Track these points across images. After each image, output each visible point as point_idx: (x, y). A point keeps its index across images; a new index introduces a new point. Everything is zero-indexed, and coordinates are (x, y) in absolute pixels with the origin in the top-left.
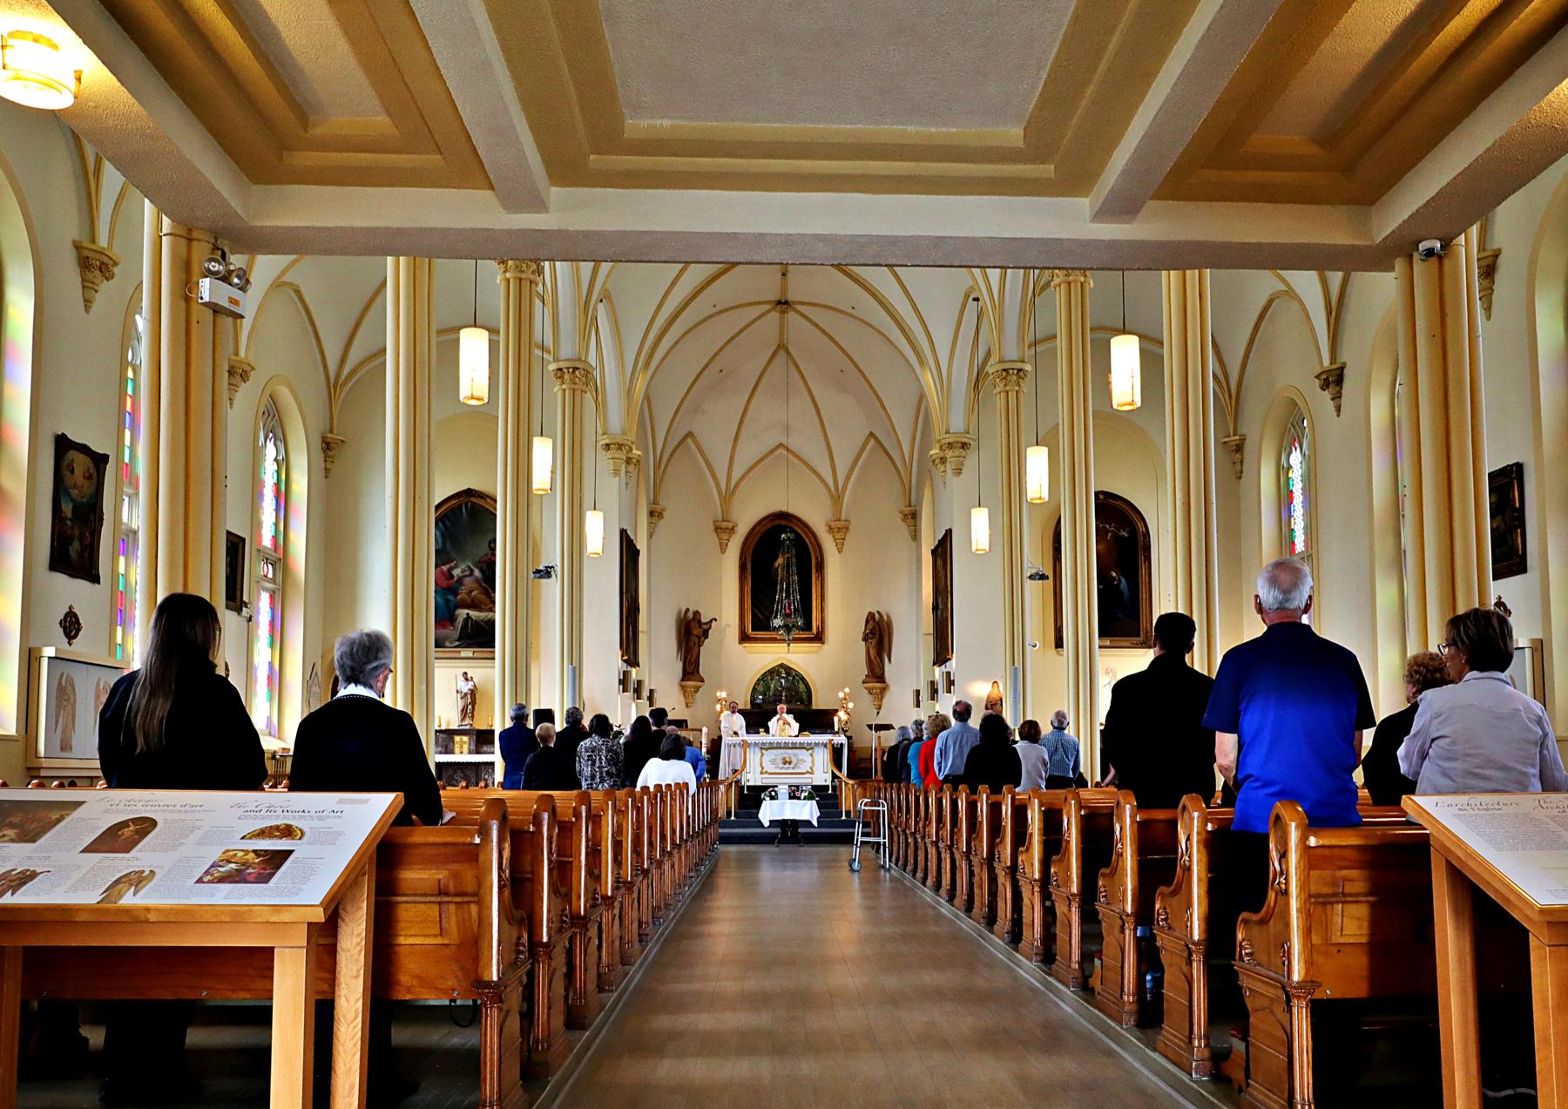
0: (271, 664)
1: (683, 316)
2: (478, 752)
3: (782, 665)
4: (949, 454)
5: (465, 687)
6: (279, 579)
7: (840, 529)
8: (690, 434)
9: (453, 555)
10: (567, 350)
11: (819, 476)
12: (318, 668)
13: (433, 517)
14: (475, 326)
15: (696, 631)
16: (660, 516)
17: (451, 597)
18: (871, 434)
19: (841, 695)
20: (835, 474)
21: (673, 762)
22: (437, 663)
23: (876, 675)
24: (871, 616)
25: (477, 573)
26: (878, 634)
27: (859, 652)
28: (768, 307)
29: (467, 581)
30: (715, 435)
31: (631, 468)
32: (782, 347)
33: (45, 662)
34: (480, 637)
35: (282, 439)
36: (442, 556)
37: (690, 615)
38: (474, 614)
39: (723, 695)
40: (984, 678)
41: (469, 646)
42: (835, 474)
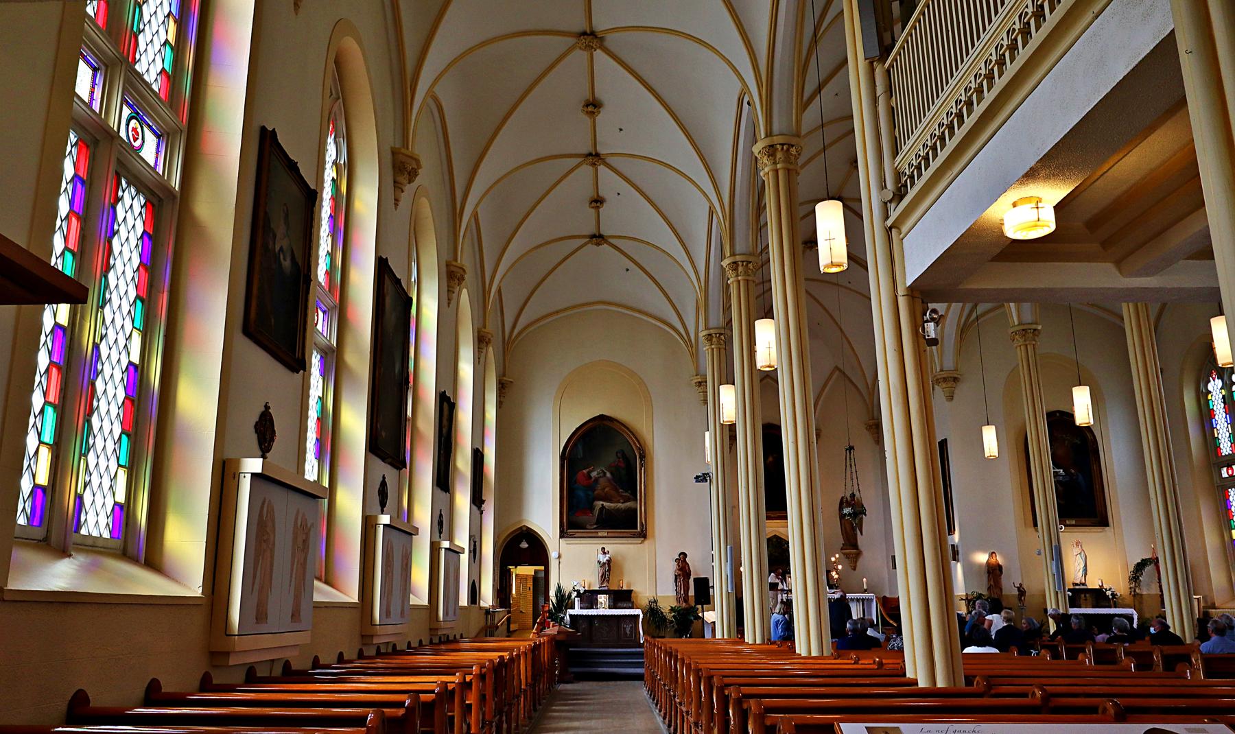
2: (616, 608)
5: (604, 559)
11: (856, 387)
20: (514, 327)
21: (255, 436)
25: (608, 475)
29: (601, 480)
33: (380, 530)
40: (984, 550)
42: (514, 327)
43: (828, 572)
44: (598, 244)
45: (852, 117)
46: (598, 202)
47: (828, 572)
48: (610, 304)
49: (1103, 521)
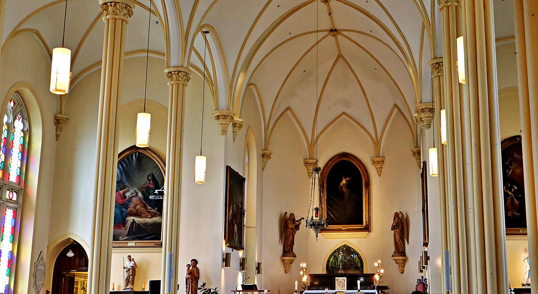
0: (12, 253)
1: (269, 39)
3: (345, 246)
4: (422, 115)
5: (129, 265)
6: (21, 201)
7: (379, 162)
8: (289, 108)
9: (127, 184)
10: (174, 62)
12: (44, 255)
13: (117, 160)
14: (63, 47)
15: (291, 226)
16: (269, 156)
17: (124, 210)
18: (395, 105)
19: (376, 265)
22: (114, 250)
23: (400, 251)
24: (396, 215)
25: (140, 195)
26: (401, 225)
27: (390, 236)
28: (326, 33)
29: (134, 199)
30: (303, 106)
31: (236, 129)
32: (340, 56)
34: (150, 234)
35: (27, 119)
36: (120, 185)
37: (288, 215)
38: (137, 220)
39: (304, 265)
41: (133, 239)
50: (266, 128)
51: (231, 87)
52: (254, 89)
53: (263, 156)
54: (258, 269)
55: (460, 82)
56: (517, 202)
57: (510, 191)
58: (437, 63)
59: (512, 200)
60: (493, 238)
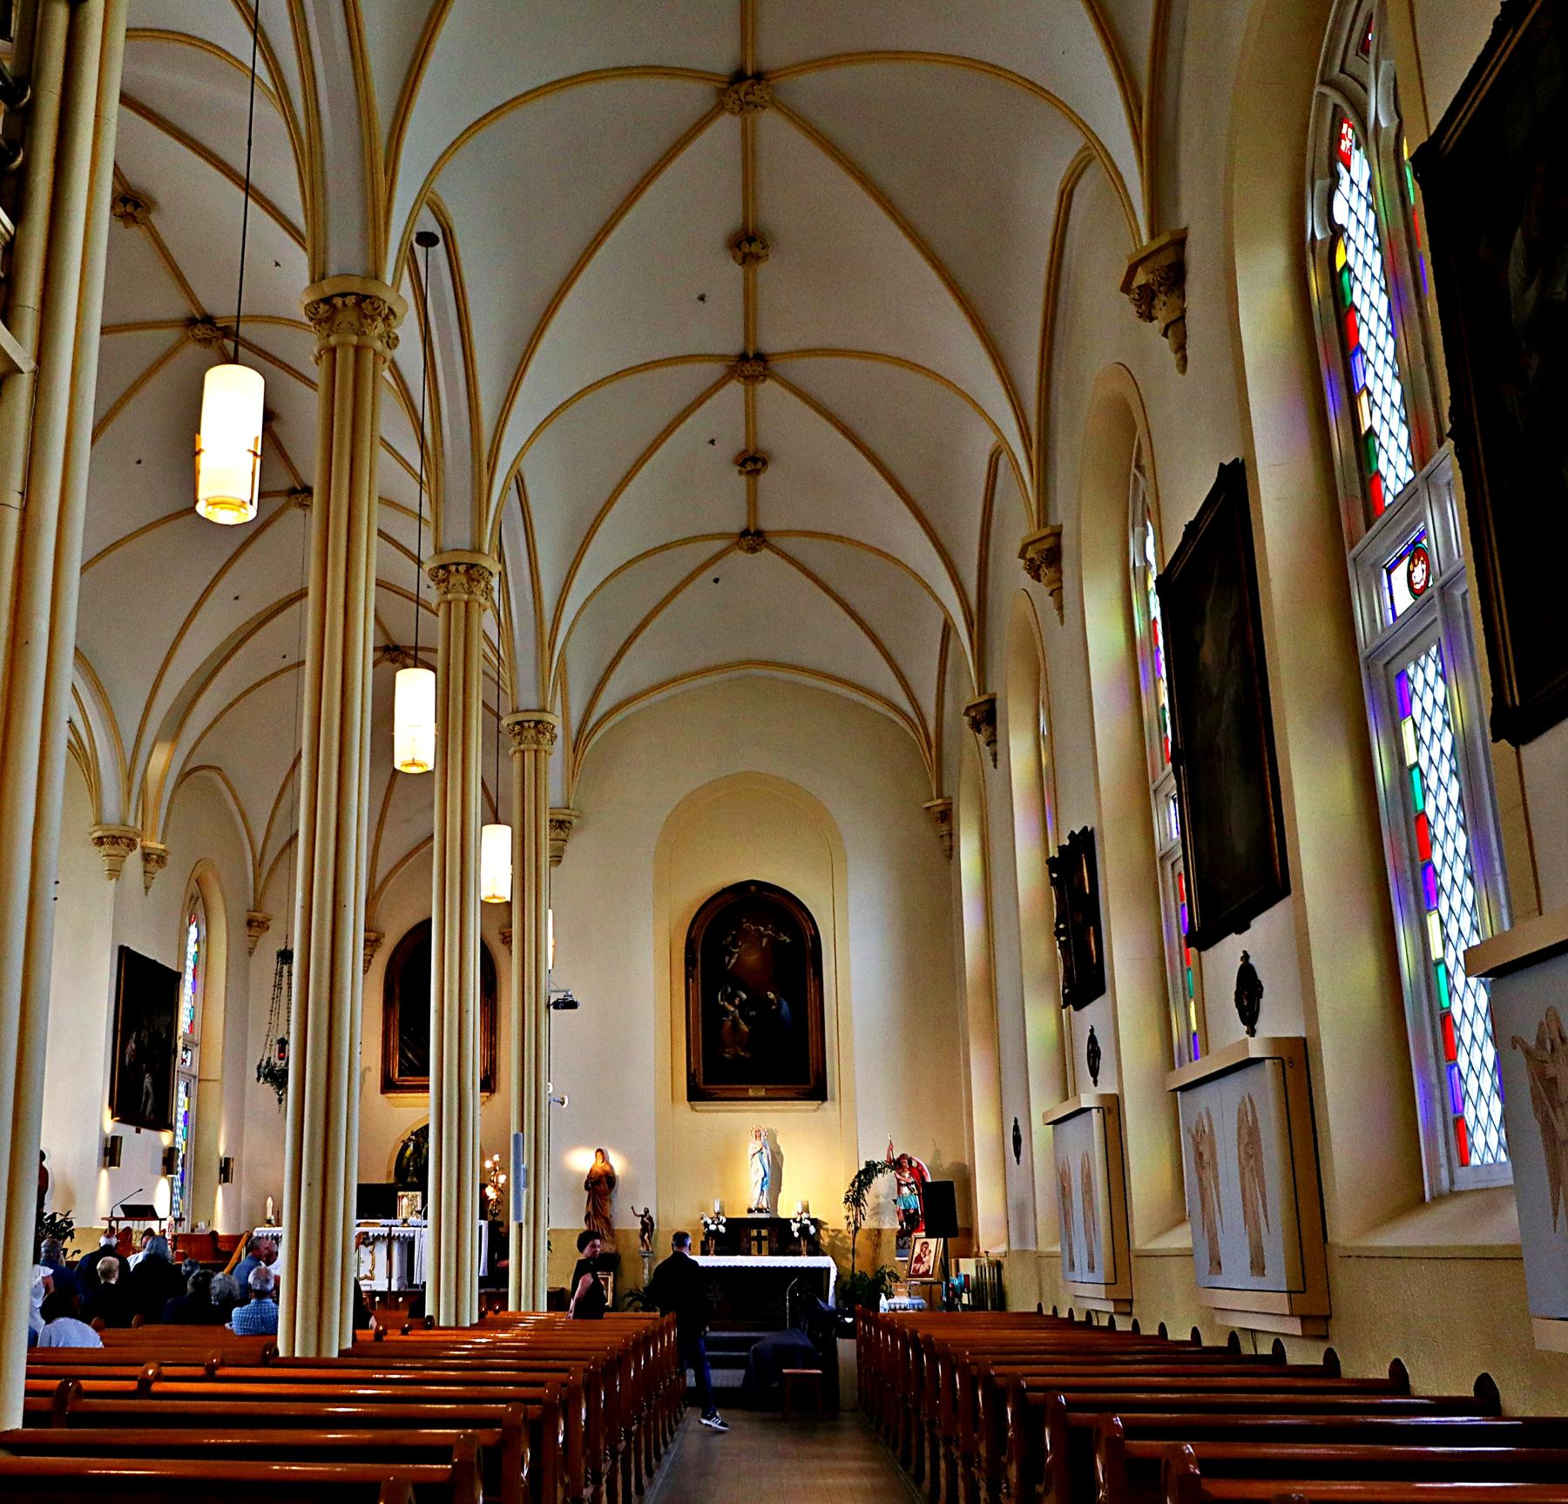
31: (152, 866)
43: (483, 1187)
44: (753, 550)
45: (104, 330)
46: (752, 462)
47: (483, 1187)
48: (804, 670)
49: (815, 1090)
50: (258, 865)
51: (129, 777)
52: (218, 779)
53: (250, 923)
54: (225, 1171)
55: (398, 766)
56: (745, 1028)
57: (732, 1003)
58: (519, 723)
59: (735, 1023)
60: (324, 1057)
